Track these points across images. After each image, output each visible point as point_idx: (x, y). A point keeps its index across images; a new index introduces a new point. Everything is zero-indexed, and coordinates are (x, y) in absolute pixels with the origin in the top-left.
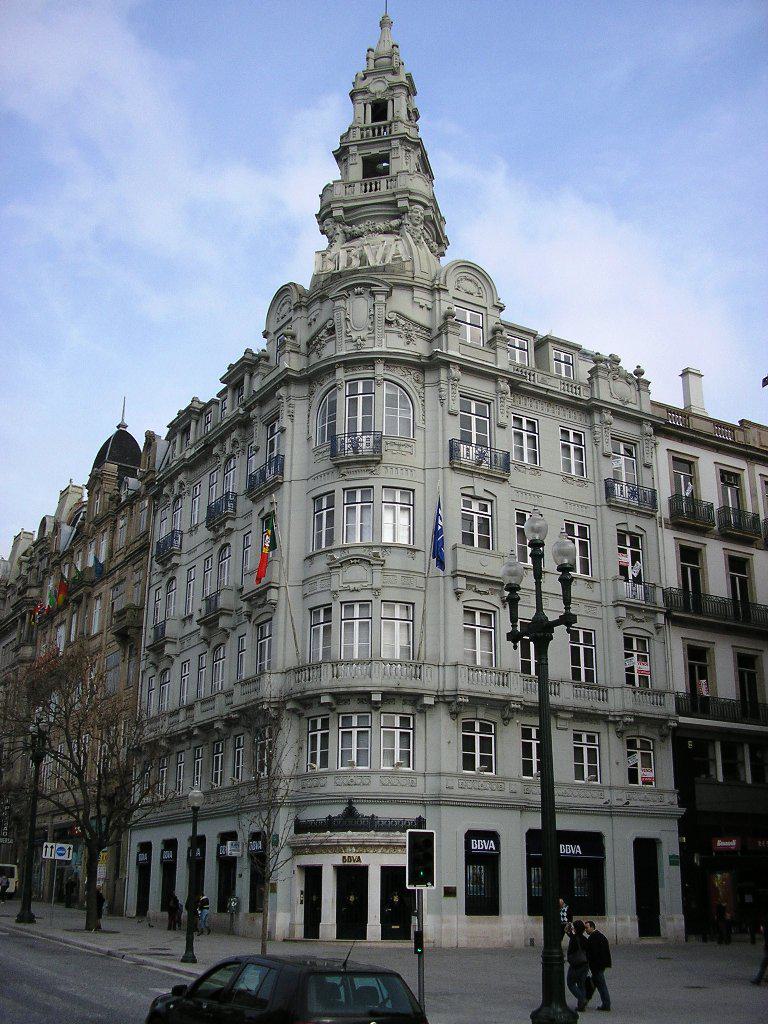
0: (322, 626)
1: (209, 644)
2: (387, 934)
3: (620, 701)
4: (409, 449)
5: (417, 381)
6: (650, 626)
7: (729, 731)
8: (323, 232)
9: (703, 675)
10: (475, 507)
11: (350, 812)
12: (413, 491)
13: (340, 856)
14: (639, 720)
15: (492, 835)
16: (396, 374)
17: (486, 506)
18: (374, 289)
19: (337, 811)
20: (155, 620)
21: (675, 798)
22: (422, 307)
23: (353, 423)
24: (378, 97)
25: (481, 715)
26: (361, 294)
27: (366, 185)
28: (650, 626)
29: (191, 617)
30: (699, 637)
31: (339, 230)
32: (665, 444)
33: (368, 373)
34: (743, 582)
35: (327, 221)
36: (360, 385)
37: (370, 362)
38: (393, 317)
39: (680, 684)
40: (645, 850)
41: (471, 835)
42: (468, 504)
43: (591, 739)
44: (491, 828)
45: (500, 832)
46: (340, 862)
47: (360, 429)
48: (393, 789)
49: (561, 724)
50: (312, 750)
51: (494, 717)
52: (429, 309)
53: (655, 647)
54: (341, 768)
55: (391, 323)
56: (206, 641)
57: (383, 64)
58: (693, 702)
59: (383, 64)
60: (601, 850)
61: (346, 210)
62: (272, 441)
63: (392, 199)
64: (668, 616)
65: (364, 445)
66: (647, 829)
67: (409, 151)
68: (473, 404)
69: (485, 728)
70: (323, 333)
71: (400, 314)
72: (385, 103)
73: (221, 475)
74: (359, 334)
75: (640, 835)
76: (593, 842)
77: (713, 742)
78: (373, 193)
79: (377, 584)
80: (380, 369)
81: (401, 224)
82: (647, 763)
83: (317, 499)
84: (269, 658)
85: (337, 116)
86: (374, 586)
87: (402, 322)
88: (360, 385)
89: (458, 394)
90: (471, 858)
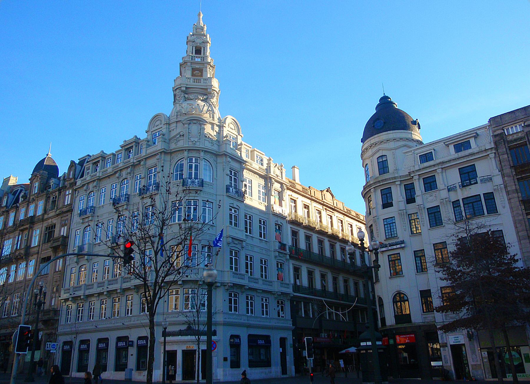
1: (78, 264)
2: (184, 378)
3: (276, 287)
6: (284, 259)
7: (306, 298)
9: (298, 278)
10: (233, 212)
11: (189, 328)
13: (186, 346)
14: (235, 285)
15: (238, 337)
16: (208, 157)
19: (184, 327)
21: (291, 323)
23: (190, 174)
24: (199, 45)
25: (235, 290)
28: (284, 259)
30: (297, 263)
31: (182, 96)
32: (291, 262)
34: (296, 240)
35: (178, 91)
36: (194, 159)
37: (198, 151)
39: (292, 281)
40: (283, 341)
41: (232, 337)
42: (231, 210)
43: (266, 300)
44: (238, 334)
45: (241, 335)
46: (185, 348)
47: (193, 177)
48: (261, 323)
49: (258, 295)
51: (238, 291)
53: (285, 267)
54: (185, 310)
56: (77, 263)
57: (198, 31)
58: (297, 288)
60: (270, 342)
61: (186, 88)
63: (206, 87)
64: (290, 256)
66: (283, 334)
69: (235, 296)
70: (178, 136)
73: (118, 186)
74: (194, 139)
75: (233, 334)
76: (267, 339)
77: (301, 302)
78: (198, 84)
80: (202, 154)
81: (207, 98)
82: (282, 310)
85: (182, 51)
88: (194, 159)
90: (232, 345)
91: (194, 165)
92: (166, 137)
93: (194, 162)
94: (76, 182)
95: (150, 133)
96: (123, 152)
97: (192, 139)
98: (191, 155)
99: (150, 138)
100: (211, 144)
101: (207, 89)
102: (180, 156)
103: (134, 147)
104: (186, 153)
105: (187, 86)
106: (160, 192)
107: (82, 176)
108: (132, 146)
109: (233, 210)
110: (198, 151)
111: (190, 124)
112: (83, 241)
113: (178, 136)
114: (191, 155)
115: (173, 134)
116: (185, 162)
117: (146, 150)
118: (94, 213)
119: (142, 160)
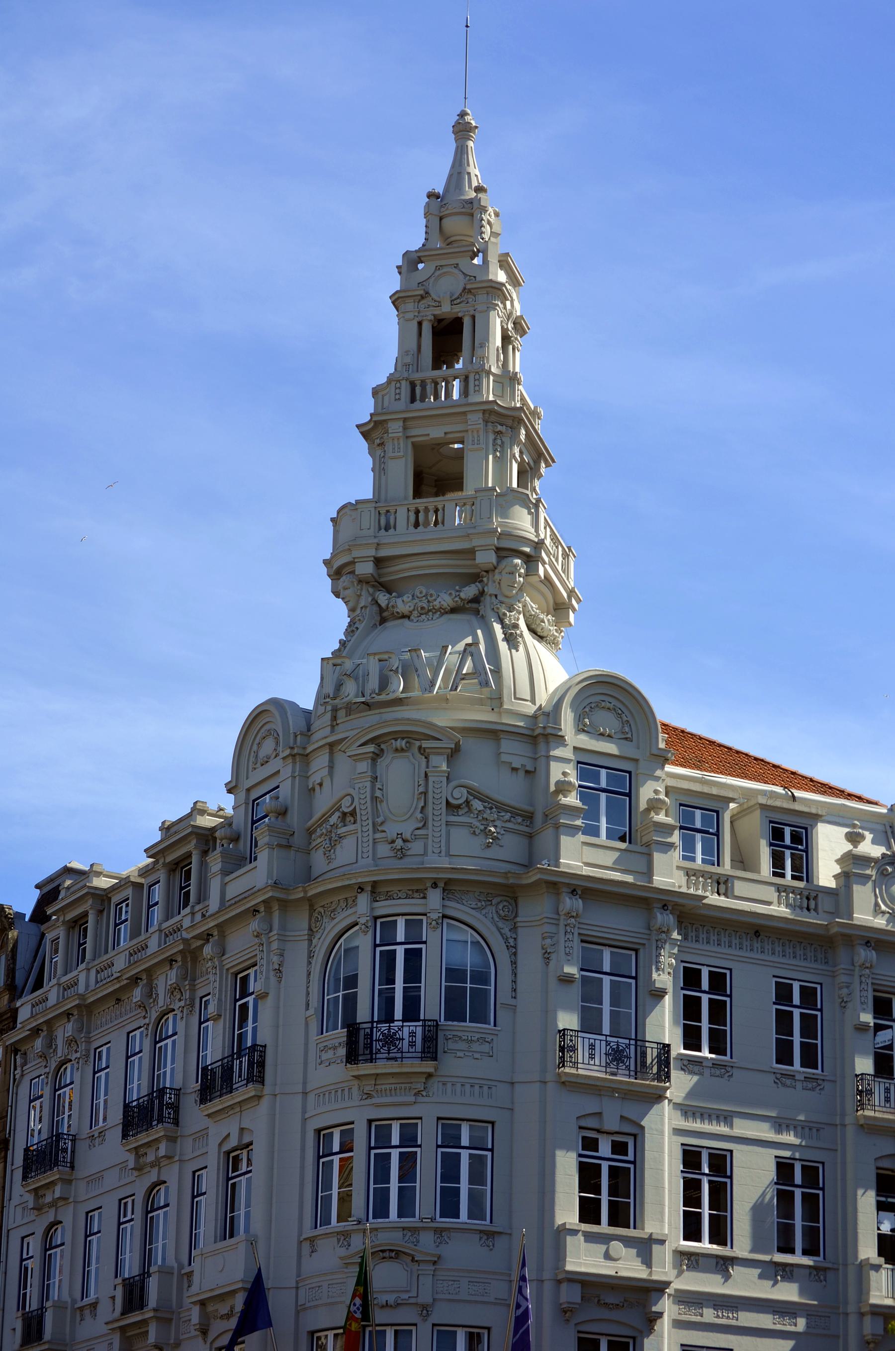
0: (336, 1159)
4: (486, 1048)
5: (504, 918)
8: (337, 594)
10: (605, 1149)
12: (493, 1123)
17: (625, 1145)
18: (426, 744)
20: (22, 1300)
22: (515, 770)
26: (402, 750)
27: (417, 512)
29: (94, 1305)
33: (413, 905)
38: (460, 796)
50: (240, 1028)
52: (527, 772)
55: (458, 807)
59: (453, 214)
62: (244, 1007)
65: (406, 1043)
67: (500, 433)
68: (607, 954)
70: (334, 819)
71: (474, 793)
72: (457, 323)
79: (425, 1298)
81: (482, 593)
83: (322, 1135)
84: (106, 1094)
86: (420, 1300)
87: (477, 805)
89: (576, 939)
91: (400, 951)
92: (294, 819)
93: (401, 937)
94: (16, 1011)
95: (243, 795)
96: (162, 875)
97: (392, 830)
98: (384, 907)
99: (241, 823)
100: (481, 840)
101: (471, 553)
102: (343, 919)
103: (91, 918)
104: (363, 900)
105: (383, 553)
106: (267, 1089)
107: (39, 984)
108: (85, 915)
109: (605, 1149)
110: (417, 888)
111: (376, 757)
112: (147, 1257)
113: (334, 819)
114: (384, 907)
115: (323, 802)
116: (363, 942)
117: (224, 885)
118: (176, 1122)
119: (207, 937)
